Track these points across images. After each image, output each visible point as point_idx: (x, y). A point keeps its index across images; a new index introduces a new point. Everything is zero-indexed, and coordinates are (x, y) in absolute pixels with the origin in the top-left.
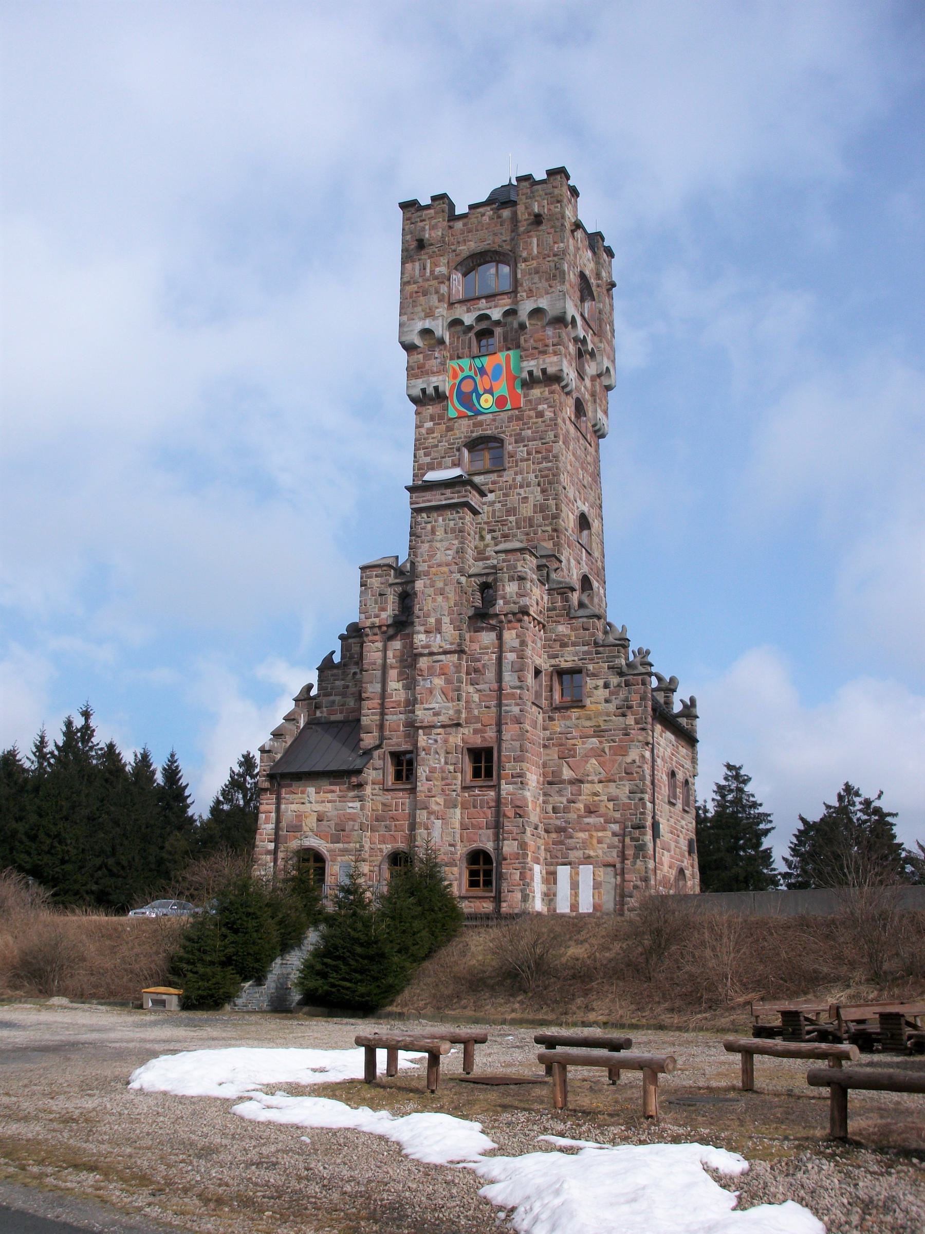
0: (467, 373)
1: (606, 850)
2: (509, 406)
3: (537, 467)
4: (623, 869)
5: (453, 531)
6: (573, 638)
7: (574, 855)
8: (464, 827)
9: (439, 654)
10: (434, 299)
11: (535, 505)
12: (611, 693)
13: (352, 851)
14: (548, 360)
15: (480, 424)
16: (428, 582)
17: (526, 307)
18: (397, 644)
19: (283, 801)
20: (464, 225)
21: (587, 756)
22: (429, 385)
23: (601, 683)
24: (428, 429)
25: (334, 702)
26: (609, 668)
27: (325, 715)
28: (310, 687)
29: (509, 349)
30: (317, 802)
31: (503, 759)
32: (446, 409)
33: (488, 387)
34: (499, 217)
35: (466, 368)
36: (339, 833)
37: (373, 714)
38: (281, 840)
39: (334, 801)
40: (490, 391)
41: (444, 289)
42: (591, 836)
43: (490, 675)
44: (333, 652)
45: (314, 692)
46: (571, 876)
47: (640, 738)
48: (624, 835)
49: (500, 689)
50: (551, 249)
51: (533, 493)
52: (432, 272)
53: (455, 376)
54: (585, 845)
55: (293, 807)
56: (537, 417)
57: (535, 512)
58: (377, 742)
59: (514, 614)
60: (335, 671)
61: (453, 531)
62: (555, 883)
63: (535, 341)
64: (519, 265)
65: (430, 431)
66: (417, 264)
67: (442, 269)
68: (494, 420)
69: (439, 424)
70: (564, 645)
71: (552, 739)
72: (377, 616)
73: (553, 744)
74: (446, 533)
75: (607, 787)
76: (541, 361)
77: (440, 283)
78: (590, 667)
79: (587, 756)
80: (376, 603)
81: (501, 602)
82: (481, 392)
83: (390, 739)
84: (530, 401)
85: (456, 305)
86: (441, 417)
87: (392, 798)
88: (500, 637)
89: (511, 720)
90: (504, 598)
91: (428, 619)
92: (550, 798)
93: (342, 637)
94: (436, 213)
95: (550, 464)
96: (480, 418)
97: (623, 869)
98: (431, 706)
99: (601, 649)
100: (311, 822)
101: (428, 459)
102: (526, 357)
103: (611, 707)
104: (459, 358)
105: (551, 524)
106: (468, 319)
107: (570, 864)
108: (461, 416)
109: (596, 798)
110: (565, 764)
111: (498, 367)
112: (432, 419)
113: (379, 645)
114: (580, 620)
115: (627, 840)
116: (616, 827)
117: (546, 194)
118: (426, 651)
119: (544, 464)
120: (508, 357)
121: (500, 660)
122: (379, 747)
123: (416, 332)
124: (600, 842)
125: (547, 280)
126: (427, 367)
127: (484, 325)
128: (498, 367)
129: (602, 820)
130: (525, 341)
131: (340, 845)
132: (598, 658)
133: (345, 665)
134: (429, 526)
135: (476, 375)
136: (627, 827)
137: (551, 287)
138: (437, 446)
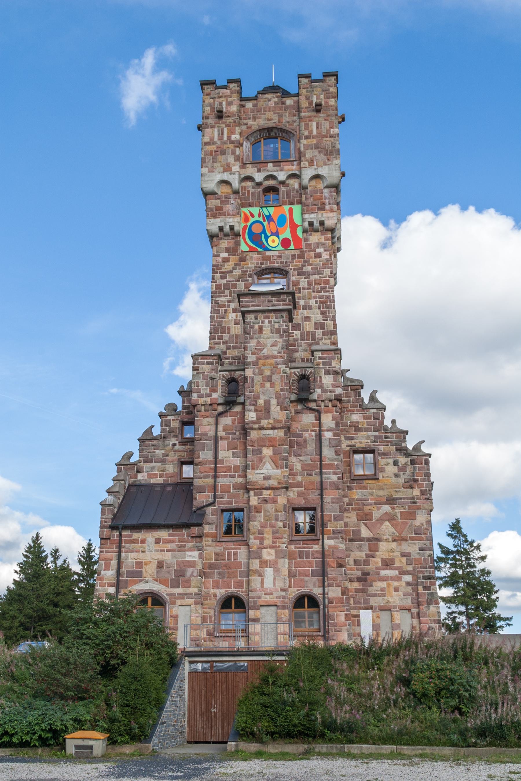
0: (256, 218)
1: (402, 597)
2: (292, 247)
3: (317, 295)
4: (418, 614)
5: (278, 331)
6: (365, 425)
7: (374, 602)
8: (291, 574)
9: (268, 429)
10: (231, 159)
11: (315, 323)
12: (400, 469)
13: (191, 594)
14: (325, 215)
15: (269, 258)
16: (257, 371)
17: (307, 173)
18: (227, 421)
19: (123, 549)
20: (254, 106)
21: (381, 520)
22: (225, 224)
23: (391, 461)
24: (224, 258)
25: (153, 468)
26: (397, 449)
27: (146, 478)
28: (129, 455)
29: (292, 203)
30: (157, 551)
31: (325, 518)
32: (238, 243)
33: (274, 231)
34: (283, 103)
35: (256, 214)
36: (179, 578)
37: (205, 477)
38: (121, 584)
39: (174, 550)
40: (277, 234)
41: (238, 151)
42: (389, 585)
43: (311, 447)
44: (153, 426)
45: (135, 458)
46: (373, 619)
47: (426, 506)
48: (417, 584)
49: (321, 460)
50: (328, 132)
51: (313, 314)
52: (229, 137)
53: (247, 220)
54: (383, 593)
55: (132, 555)
56: (315, 257)
57: (316, 329)
58: (211, 500)
59: (331, 401)
60: (155, 442)
61: (278, 331)
62: (359, 625)
63: (314, 199)
64: (301, 141)
65: (226, 260)
66: (216, 130)
67: (235, 137)
68: (280, 256)
69: (234, 255)
70: (358, 430)
71: (351, 504)
72: (209, 396)
73: (352, 508)
74: (272, 332)
75: (400, 545)
76: (320, 215)
77: (235, 146)
78: (382, 448)
79: (381, 520)
80: (207, 385)
81: (319, 391)
82: (269, 235)
83: (222, 498)
84: (310, 245)
85: (248, 165)
86: (235, 250)
87: (225, 549)
88: (318, 419)
89: (331, 486)
90: (321, 387)
91: (258, 400)
92: (352, 553)
93: (161, 415)
94: (231, 93)
95: (327, 294)
96: (268, 253)
97: (418, 614)
98: (262, 471)
99: (389, 434)
100: (150, 570)
101: (224, 282)
102: (307, 210)
103: (401, 481)
104: (250, 206)
105: (330, 339)
106: (259, 177)
107: (371, 608)
108: (252, 250)
109: (391, 554)
110: (363, 526)
111: (282, 218)
112: (227, 250)
113: (212, 420)
114: (371, 411)
115: (420, 588)
116: (408, 578)
117: (323, 91)
118: (256, 426)
119: (323, 294)
120: (291, 210)
121: (319, 437)
122: (212, 504)
123: (216, 182)
124: (396, 590)
125: (325, 155)
126: (224, 210)
127: (271, 183)
128: (282, 218)
129: (397, 572)
130: (306, 199)
131: (180, 590)
132: (387, 442)
133: (164, 437)
134: (257, 326)
135: (264, 221)
136: (419, 578)
137: (328, 160)
138: (231, 272)
